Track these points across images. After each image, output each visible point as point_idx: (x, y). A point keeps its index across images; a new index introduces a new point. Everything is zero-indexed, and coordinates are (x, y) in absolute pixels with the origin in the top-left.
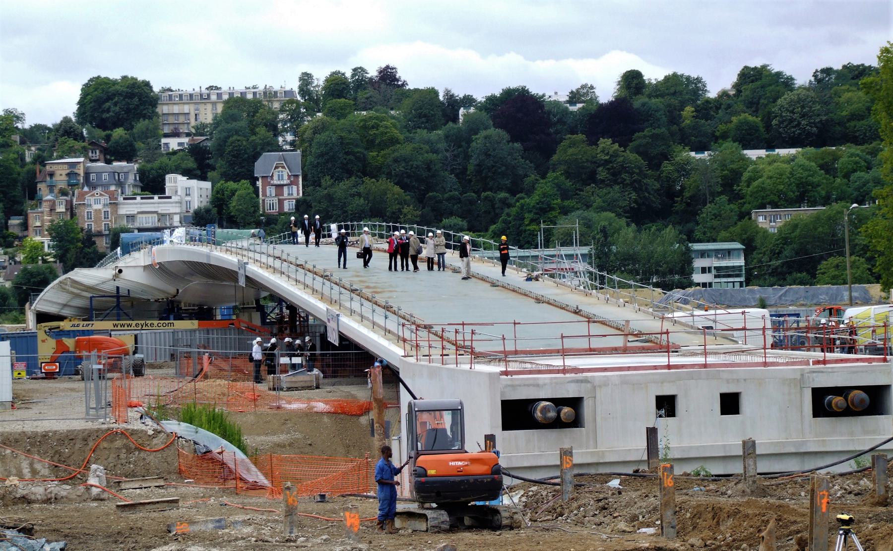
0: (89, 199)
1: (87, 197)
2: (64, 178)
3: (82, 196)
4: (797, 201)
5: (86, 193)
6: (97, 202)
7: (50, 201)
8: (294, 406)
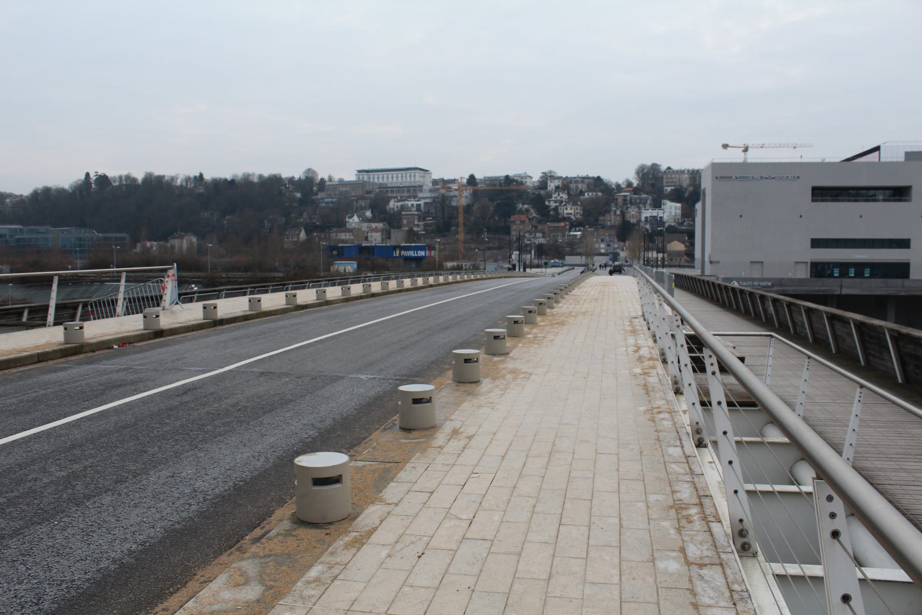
0: (630, 210)
1: (629, 209)
2: (621, 201)
3: (627, 208)
4: (82, 225)
5: (629, 207)
6: (633, 211)
7: (614, 210)
8: (3, 321)
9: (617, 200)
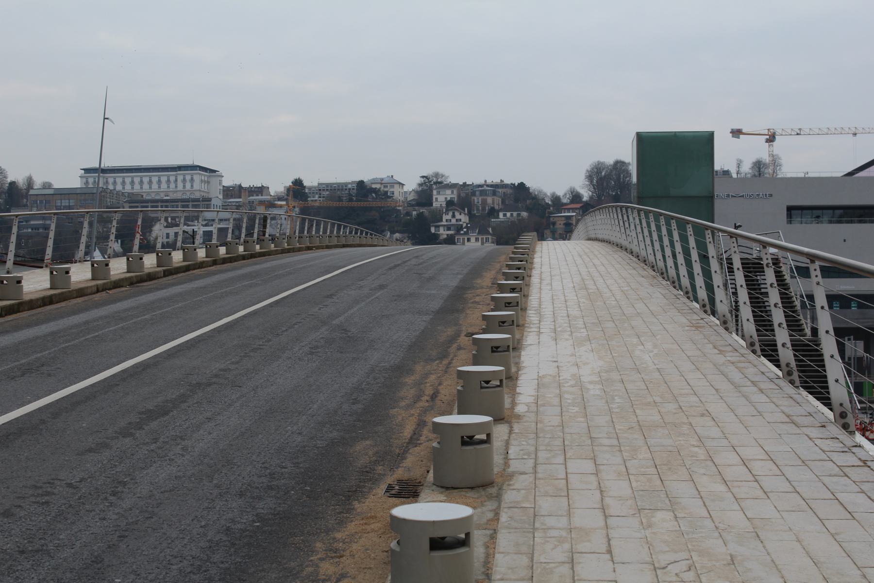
9: (554, 224)
